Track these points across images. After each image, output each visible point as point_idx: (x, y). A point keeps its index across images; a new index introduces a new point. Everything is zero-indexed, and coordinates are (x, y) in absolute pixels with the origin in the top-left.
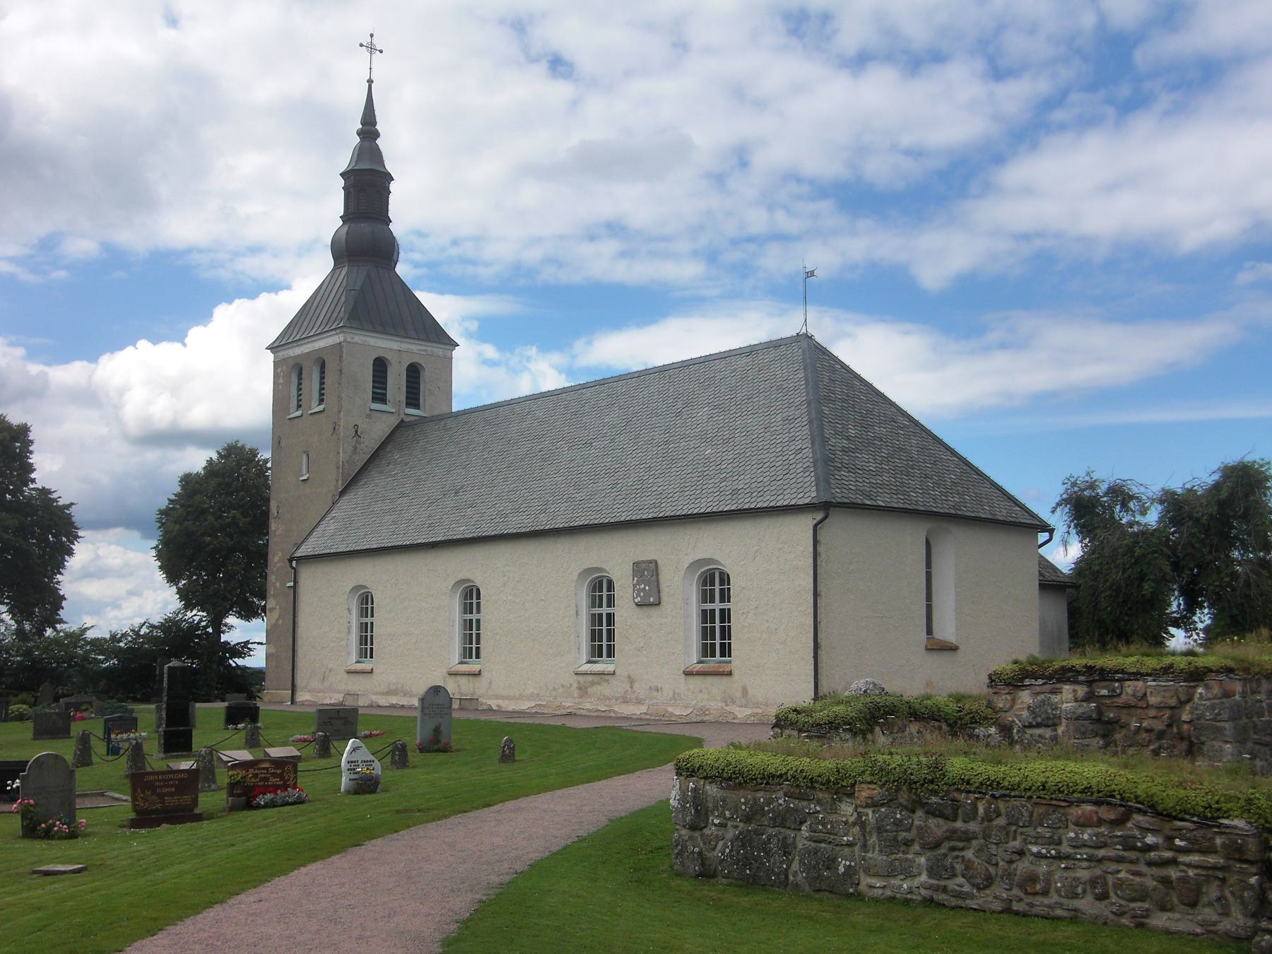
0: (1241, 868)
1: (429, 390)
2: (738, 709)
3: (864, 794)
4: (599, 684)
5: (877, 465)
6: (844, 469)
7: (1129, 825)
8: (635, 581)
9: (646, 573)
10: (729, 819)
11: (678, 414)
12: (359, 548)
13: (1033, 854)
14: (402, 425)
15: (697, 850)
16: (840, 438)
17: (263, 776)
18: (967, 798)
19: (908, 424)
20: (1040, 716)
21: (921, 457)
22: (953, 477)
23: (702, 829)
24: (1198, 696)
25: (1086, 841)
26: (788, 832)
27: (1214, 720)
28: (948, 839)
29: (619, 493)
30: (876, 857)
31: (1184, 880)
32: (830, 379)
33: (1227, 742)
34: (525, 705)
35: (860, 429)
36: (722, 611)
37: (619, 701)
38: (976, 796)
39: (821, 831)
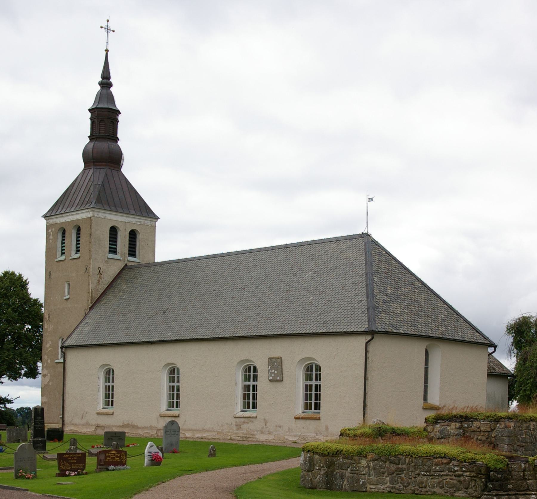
1: (142, 246)
3: (370, 457)
4: (248, 423)
5: (402, 310)
6: (383, 312)
8: (269, 368)
9: (275, 364)
10: (322, 467)
11: (295, 275)
12: (106, 343)
13: (422, 475)
14: (126, 267)
15: (310, 479)
16: (382, 295)
18: (403, 457)
19: (420, 286)
20: (443, 434)
21: (426, 305)
22: (443, 316)
24: (497, 427)
26: (343, 471)
27: (502, 436)
28: (396, 471)
29: (261, 319)
30: (373, 478)
31: (465, 480)
32: (379, 260)
33: (506, 444)
35: (393, 289)
36: (316, 386)
37: (259, 432)
39: (355, 470)
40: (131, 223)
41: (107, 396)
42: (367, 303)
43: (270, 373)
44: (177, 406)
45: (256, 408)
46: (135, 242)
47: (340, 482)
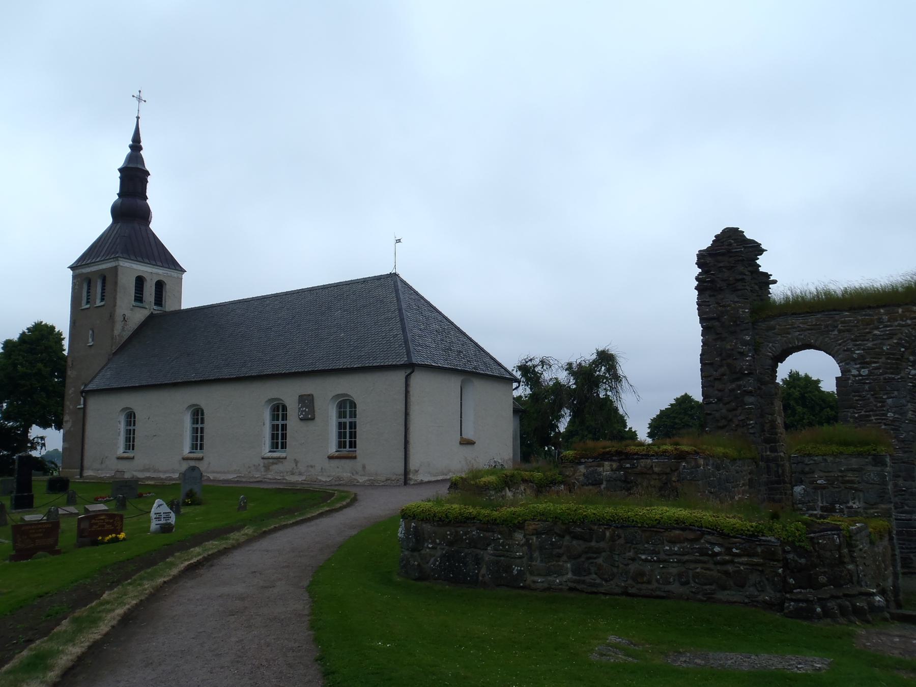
0: (773, 564)
2: (360, 477)
4: (276, 464)
7: (702, 541)
8: (300, 406)
10: (439, 544)
13: (642, 560)
14: (151, 317)
15: (416, 563)
17: (101, 524)
23: (419, 551)
25: (676, 551)
26: (478, 551)
30: (538, 563)
34: (230, 477)
37: (288, 473)
38: (605, 527)
39: (501, 550)
40: (158, 274)
41: (128, 440)
42: (403, 336)
43: (301, 411)
44: (201, 448)
45: (286, 448)
46: (162, 292)
47: (475, 569)
